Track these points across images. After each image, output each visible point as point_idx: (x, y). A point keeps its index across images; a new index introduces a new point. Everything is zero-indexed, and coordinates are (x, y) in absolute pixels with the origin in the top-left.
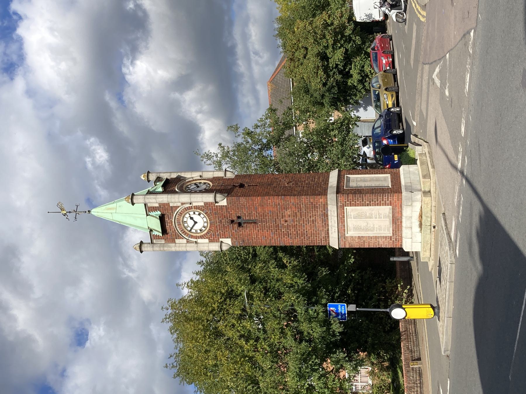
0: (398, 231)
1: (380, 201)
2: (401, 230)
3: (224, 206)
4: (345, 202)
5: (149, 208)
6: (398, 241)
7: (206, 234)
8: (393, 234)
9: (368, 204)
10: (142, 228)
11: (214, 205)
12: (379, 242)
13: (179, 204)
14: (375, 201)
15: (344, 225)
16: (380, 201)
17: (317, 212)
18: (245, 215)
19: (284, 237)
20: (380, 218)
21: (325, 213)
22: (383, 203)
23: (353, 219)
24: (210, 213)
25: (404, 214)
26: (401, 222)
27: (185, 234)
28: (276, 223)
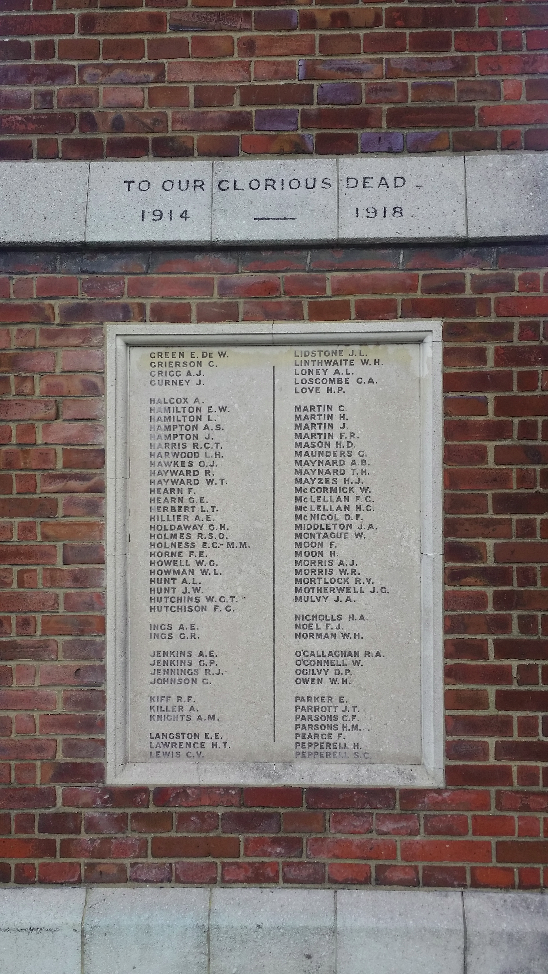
0: (163, 849)
1: (499, 675)
2: (168, 878)
4: (499, 331)
6: (48, 849)
8: (133, 794)
9: (474, 553)
12: (38, 651)
15: (229, 314)
16: (499, 675)
17: (377, 44)
20: (307, 668)
21: (363, 119)
22: (478, 701)
23: (288, 401)
26: (259, 877)
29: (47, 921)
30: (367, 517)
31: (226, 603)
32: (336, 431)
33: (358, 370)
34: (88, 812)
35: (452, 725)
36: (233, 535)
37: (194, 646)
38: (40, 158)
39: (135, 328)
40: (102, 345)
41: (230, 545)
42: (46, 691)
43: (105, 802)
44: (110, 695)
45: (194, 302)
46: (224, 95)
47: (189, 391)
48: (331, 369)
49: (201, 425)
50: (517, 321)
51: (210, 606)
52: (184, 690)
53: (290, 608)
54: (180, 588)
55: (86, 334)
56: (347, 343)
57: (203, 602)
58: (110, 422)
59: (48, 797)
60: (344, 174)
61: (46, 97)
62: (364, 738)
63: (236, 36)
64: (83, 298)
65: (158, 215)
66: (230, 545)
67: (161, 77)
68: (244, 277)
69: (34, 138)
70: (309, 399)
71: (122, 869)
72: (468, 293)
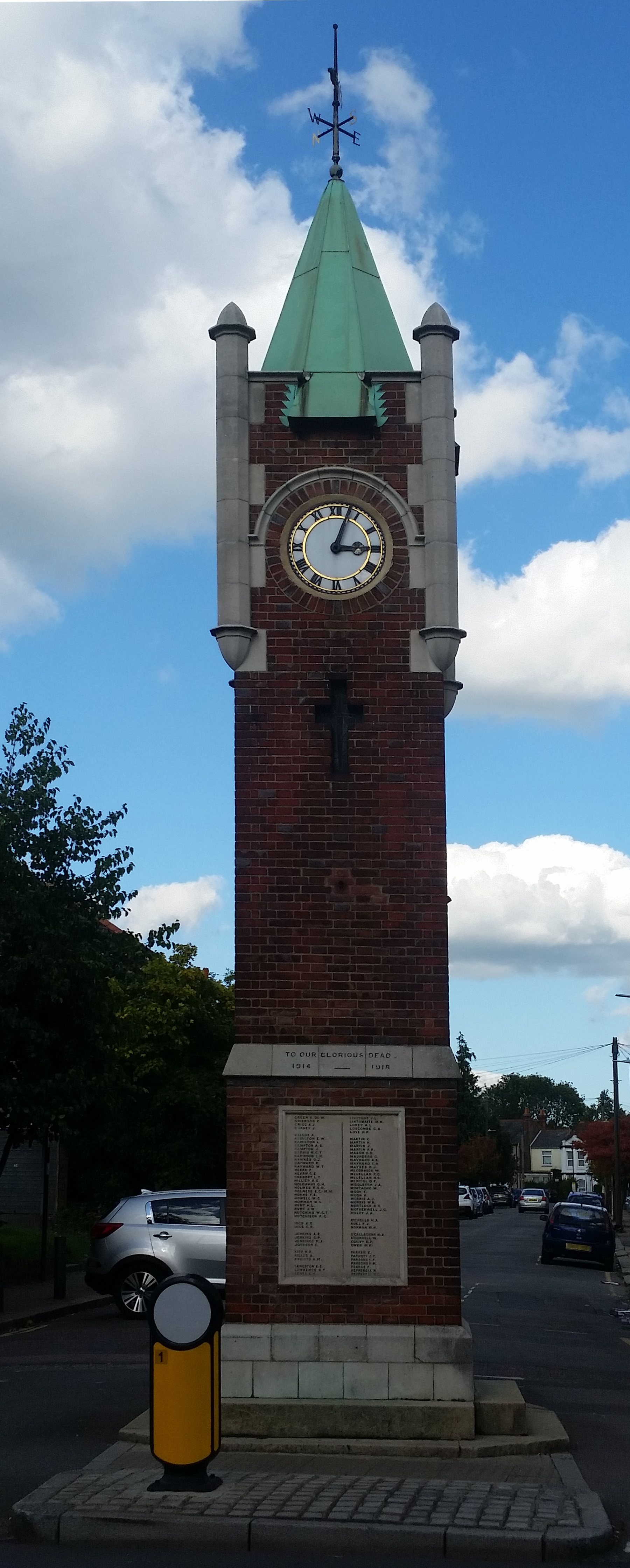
2: (303, 1321)
3: (407, 660)
4: (426, 1112)
5: (401, 386)
7: (288, 582)
8: (290, 1287)
9: (419, 1195)
10: (307, 354)
11: (413, 627)
13: (415, 498)
14: (428, 1223)
17: (379, 1005)
18: (368, 736)
19: (272, 872)
20: (355, 1240)
22: (420, 1252)
23: (348, 1136)
24: (379, 608)
25: (375, 1331)
26: (337, 1321)
27: (286, 503)
28: (330, 846)
29: (257, 1334)
30: (378, 1182)
31: (324, 1214)
32: (366, 1148)
33: (374, 1125)
34: (271, 1295)
35: (410, 1262)
36: (326, 1188)
37: (312, 1231)
38: (254, 1043)
39: (289, 1108)
40: (277, 1114)
41: (326, 1191)
42: (255, 1247)
43: (278, 1292)
44: (280, 1249)
45: (312, 1098)
46: (323, 1022)
47: (310, 1132)
48: (364, 1124)
49: (314, 1144)
50: (432, 1108)
51: (318, 1215)
52: (308, 1248)
53: (349, 1216)
54: (306, 1208)
55: (271, 1110)
56: (370, 1115)
57: (315, 1214)
58: (280, 1143)
59: (256, 1289)
60: (368, 1052)
61: (256, 1020)
62: (378, 1268)
63: (327, 1000)
64: (270, 1096)
65: (299, 1066)
66: (326, 1191)
67: (299, 1014)
68: (331, 1089)
69: (251, 1035)
70: (356, 1135)
71: (285, 1317)
72: (414, 1098)
